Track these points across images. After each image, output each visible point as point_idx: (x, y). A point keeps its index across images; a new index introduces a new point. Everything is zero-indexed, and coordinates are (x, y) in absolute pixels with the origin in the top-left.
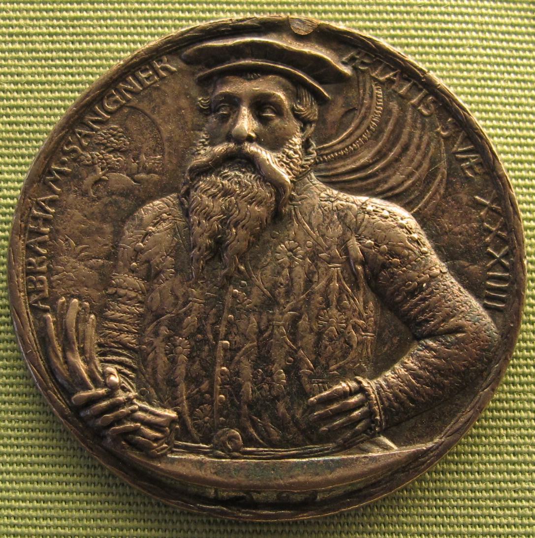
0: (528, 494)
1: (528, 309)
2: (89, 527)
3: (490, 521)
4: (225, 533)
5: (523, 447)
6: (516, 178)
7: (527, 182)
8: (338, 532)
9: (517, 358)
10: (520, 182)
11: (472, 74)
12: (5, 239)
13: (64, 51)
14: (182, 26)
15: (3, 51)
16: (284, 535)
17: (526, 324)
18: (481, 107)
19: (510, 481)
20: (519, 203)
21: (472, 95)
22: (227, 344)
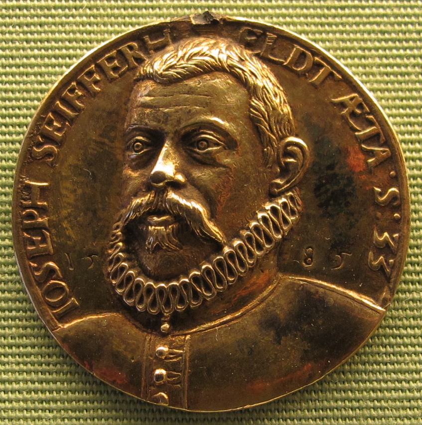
0: (416, 376)
1: (15, 155)
2: (355, 417)
3: (370, 404)
4: (177, 422)
5: (405, 338)
6: (403, 133)
7: (414, 137)
8: (262, 419)
9: (410, 273)
10: (407, 137)
11: (361, 27)
12: (6, 213)
13: (28, 91)
14: (103, 40)
15: (4, 117)
16: (229, 422)
17: (415, 222)
18: (371, 19)
19: (411, 345)
20: (406, 159)
21: (365, 41)
22: (179, 306)
